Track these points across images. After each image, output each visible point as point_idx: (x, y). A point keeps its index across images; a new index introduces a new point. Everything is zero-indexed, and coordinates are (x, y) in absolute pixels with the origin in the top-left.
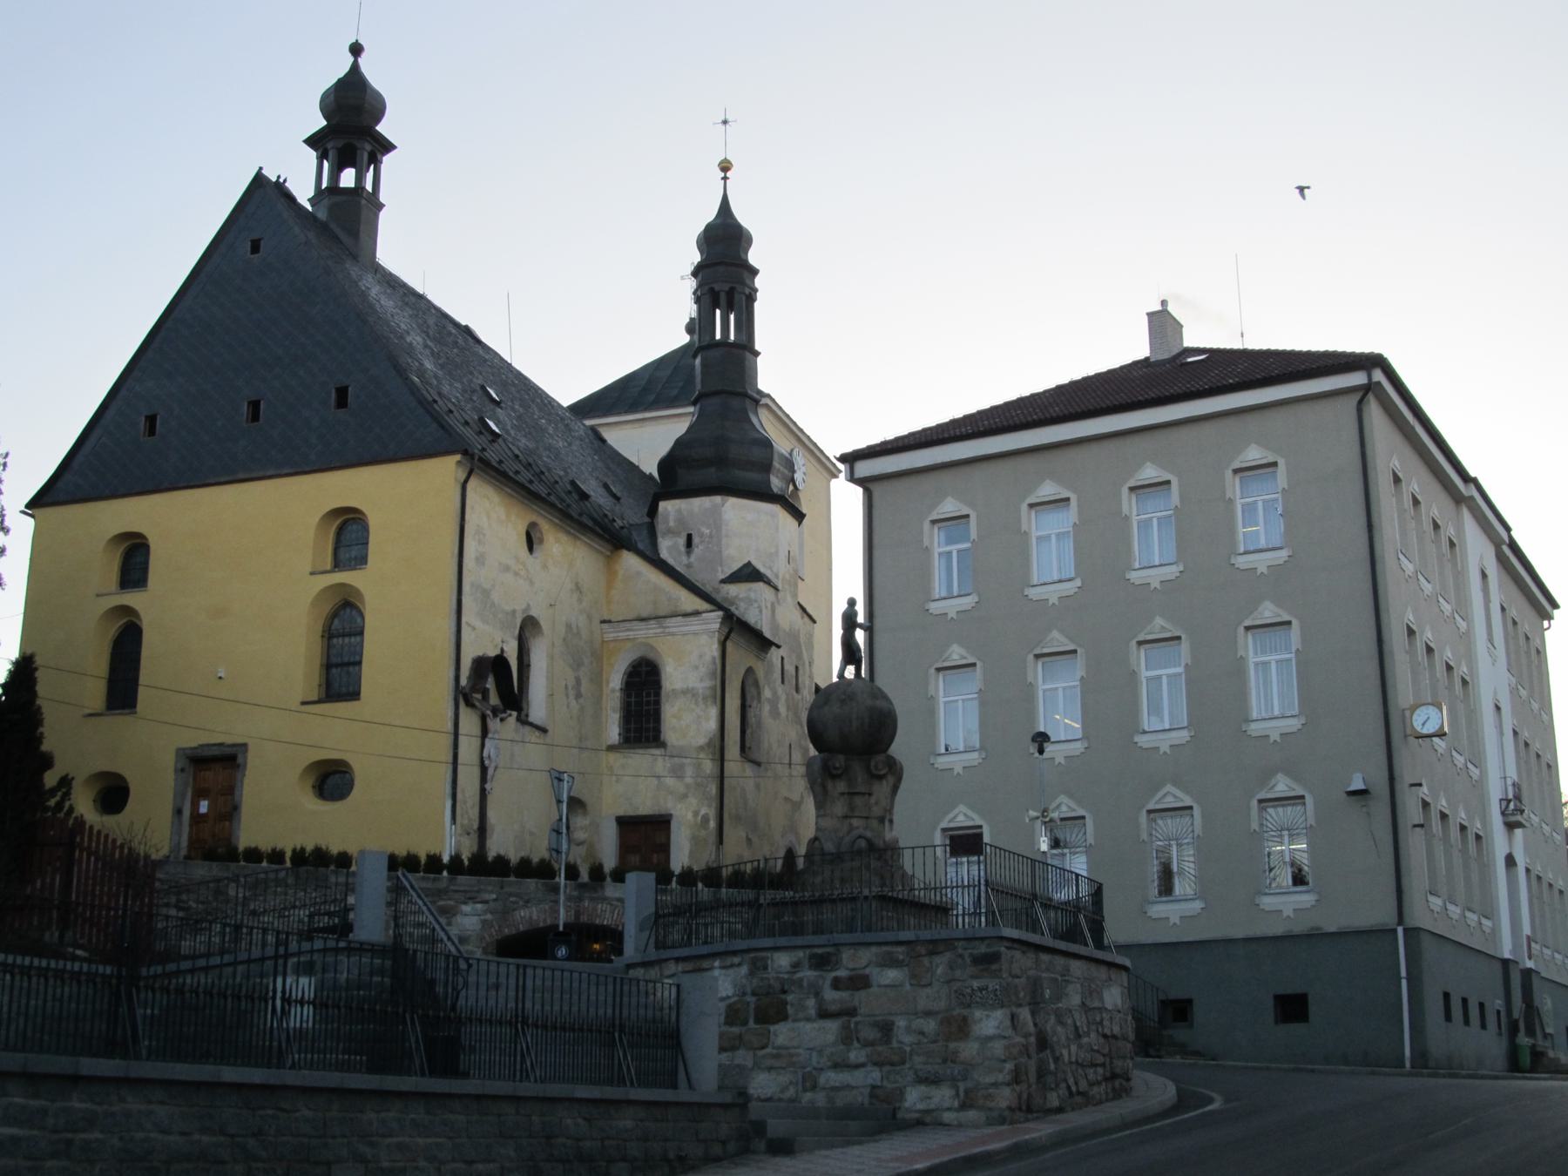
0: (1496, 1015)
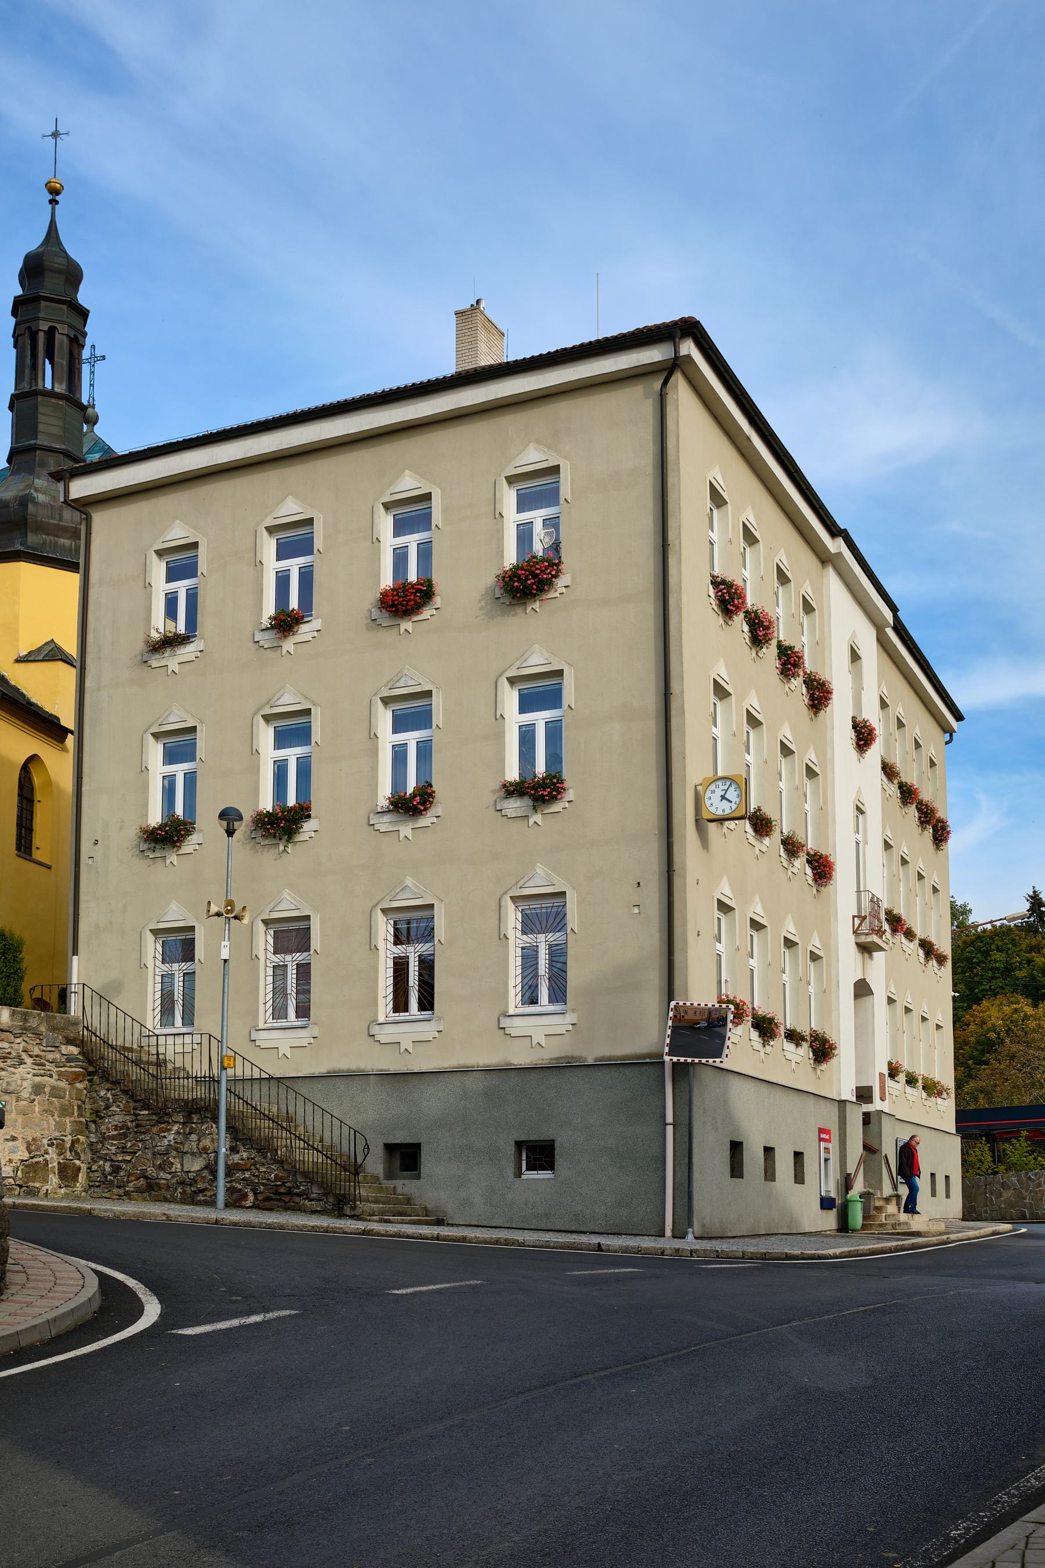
0: (727, 1153)
